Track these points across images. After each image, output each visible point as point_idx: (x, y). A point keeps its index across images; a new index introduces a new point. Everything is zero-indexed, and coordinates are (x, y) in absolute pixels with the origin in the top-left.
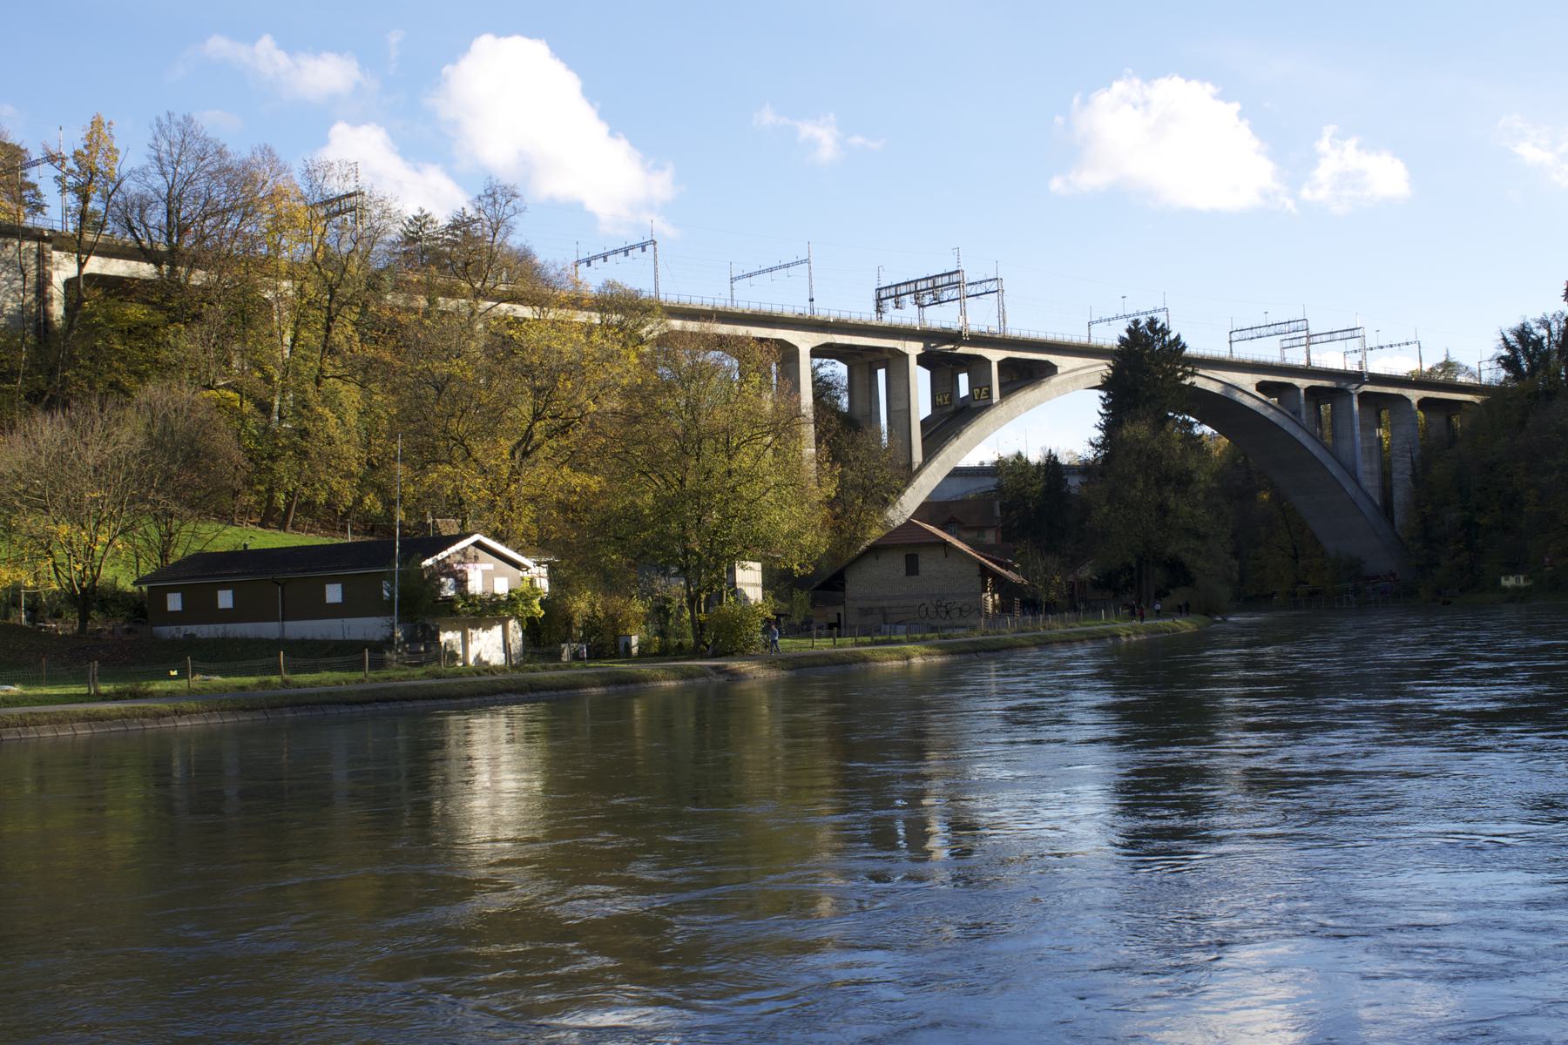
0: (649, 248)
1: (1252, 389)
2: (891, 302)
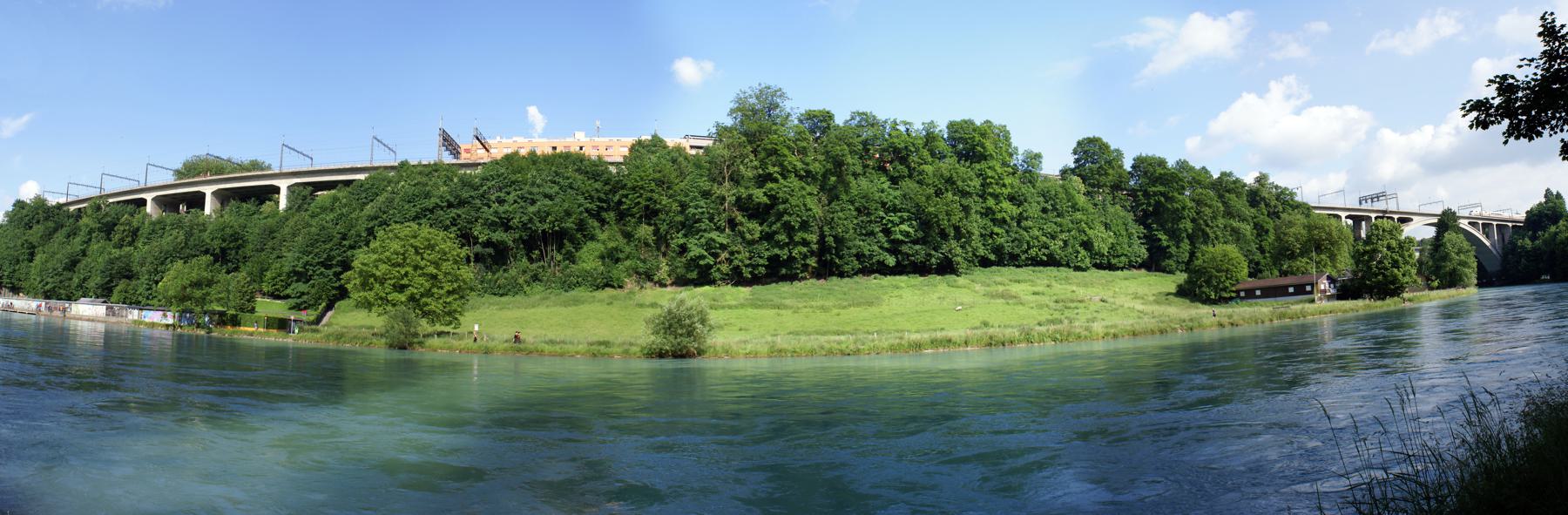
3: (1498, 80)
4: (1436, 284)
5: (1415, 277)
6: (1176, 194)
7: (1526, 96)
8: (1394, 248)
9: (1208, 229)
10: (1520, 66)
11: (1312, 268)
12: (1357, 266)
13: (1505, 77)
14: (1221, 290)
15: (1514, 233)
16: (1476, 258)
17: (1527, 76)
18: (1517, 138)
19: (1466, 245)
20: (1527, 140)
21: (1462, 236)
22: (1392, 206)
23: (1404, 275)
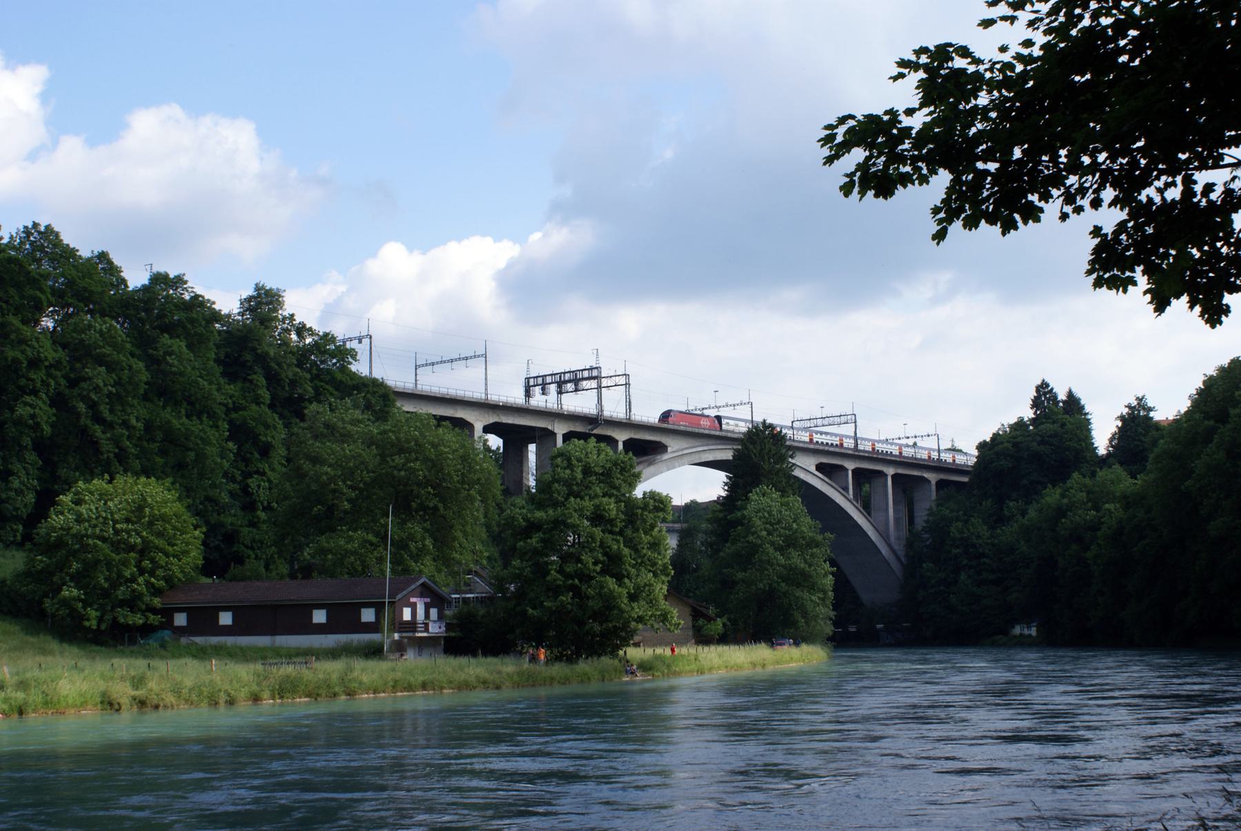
0: (366, 341)
1: (813, 469)
2: (538, 390)
3: (924, 59)
4: (718, 626)
5: (664, 604)
6: (15, 321)
7: (995, 105)
8: (611, 522)
9: (97, 430)
10: (987, 23)
11: (381, 560)
12: (506, 565)
13: (942, 53)
14: (122, 604)
15: (940, 502)
16: (833, 563)
17: (1003, 49)
18: (971, 223)
19: (807, 525)
20: (997, 229)
21: (796, 501)
22: (614, 407)
23: (633, 597)
